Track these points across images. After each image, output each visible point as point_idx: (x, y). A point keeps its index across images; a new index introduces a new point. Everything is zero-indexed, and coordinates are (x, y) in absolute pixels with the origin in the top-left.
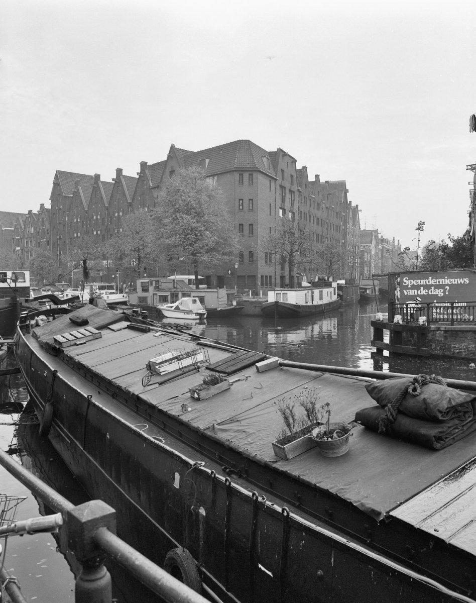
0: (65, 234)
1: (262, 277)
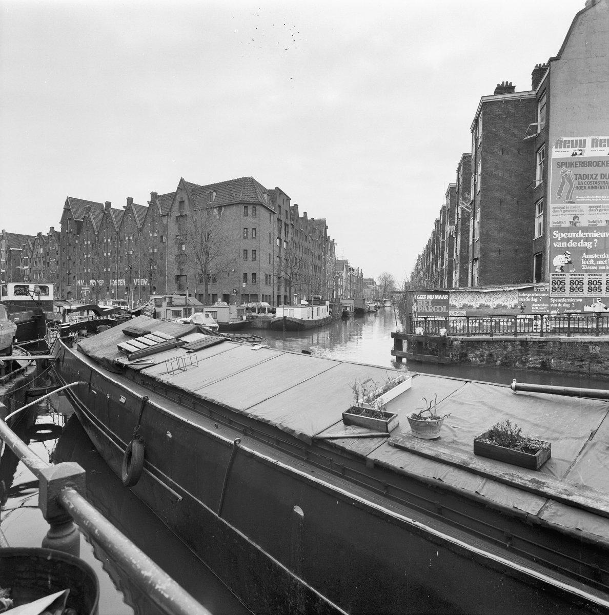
0: (75, 256)
1: (263, 295)
